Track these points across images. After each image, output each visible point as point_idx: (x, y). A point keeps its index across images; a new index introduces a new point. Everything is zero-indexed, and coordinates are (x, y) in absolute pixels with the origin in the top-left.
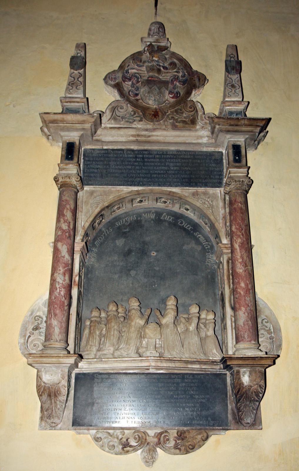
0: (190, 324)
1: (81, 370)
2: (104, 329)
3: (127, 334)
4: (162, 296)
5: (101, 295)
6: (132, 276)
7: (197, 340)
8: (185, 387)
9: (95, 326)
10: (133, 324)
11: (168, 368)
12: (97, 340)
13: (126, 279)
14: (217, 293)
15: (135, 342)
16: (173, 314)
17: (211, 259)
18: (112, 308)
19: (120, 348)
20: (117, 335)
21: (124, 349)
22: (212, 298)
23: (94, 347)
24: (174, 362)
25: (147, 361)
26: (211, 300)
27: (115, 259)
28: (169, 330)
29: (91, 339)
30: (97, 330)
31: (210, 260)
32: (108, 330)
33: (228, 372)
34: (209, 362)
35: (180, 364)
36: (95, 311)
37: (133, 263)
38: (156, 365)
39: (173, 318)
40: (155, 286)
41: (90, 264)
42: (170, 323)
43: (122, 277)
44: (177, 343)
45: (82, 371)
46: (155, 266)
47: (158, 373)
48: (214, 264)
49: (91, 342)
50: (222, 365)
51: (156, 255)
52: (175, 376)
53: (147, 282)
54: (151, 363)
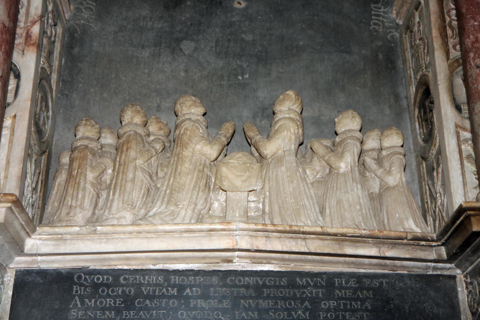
0: (341, 156)
1: (33, 262)
2: (110, 171)
3: (169, 180)
4: (261, 99)
5: (105, 95)
6: (187, 53)
7: (360, 194)
8: (336, 310)
9: (84, 158)
10: (187, 153)
11: (287, 256)
12: (87, 194)
13: (169, 59)
14: (403, 95)
15: (191, 198)
16: (292, 131)
17: (383, 17)
18: (132, 119)
19: (151, 213)
20: (142, 181)
21: (162, 216)
22: (390, 106)
23: (78, 210)
24: (305, 239)
25: (226, 235)
26: (387, 111)
27: (143, 13)
28: (283, 169)
29: (70, 191)
30: (89, 168)
31: (381, 19)
32: (119, 169)
33: (459, 271)
34: (406, 238)
35: (320, 242)
36: (86, 125)
37: (189, 23)
38: (252, 245)
39: (293, 141)
40: (243, 76)
41: (79, 25)
42: (286, 153)
43: (160, 55)
44: (307, 203)
45: (37, 262)
46: (243, 32)
47: (256, 272)
48: (391, 28)
49: (70, 200)
50: (443, 249)
51: (246, 8)
52: (307, 281)
53: (222, 68)
54: (239, 241)
